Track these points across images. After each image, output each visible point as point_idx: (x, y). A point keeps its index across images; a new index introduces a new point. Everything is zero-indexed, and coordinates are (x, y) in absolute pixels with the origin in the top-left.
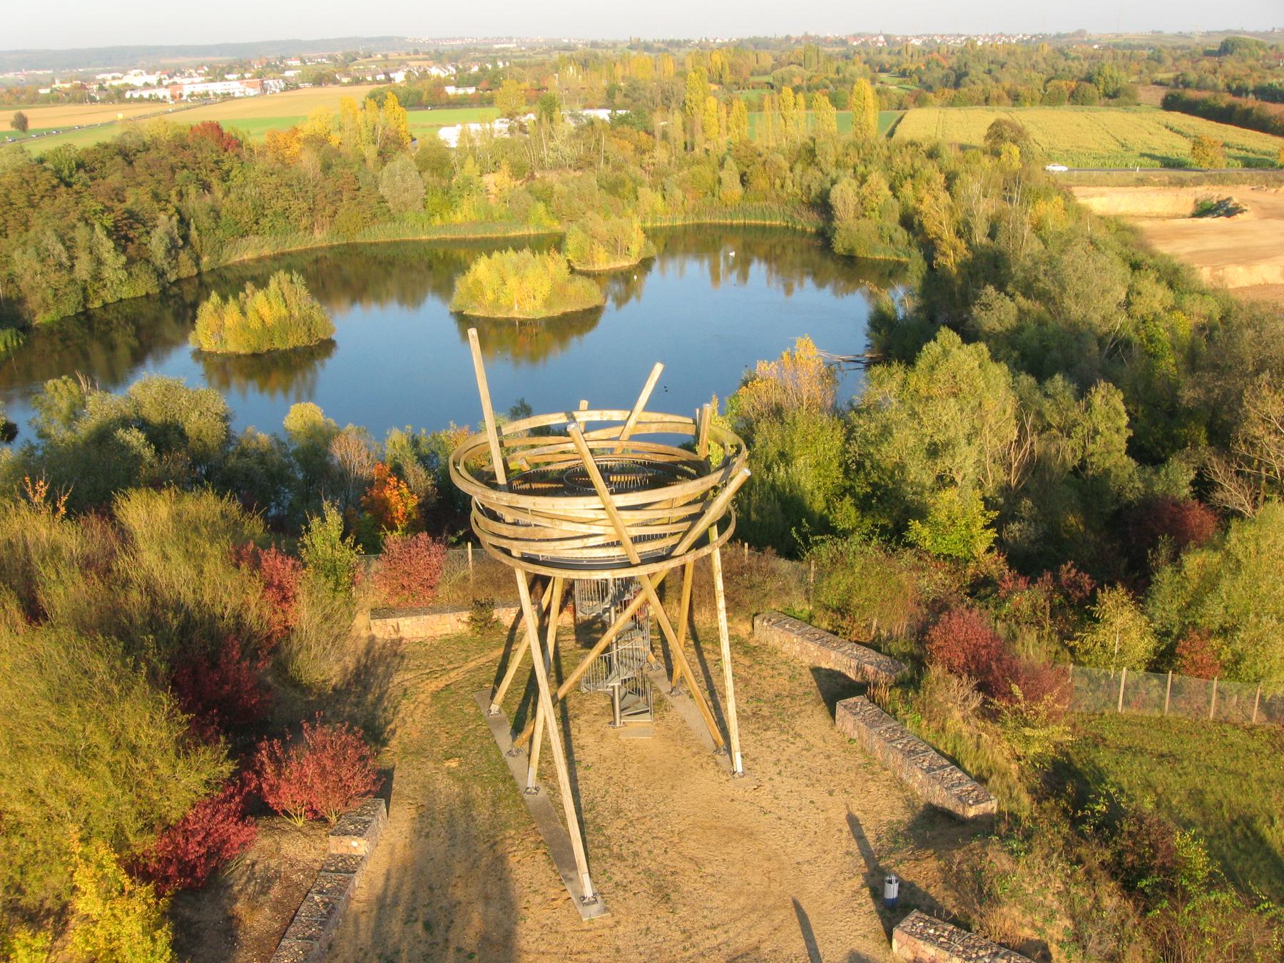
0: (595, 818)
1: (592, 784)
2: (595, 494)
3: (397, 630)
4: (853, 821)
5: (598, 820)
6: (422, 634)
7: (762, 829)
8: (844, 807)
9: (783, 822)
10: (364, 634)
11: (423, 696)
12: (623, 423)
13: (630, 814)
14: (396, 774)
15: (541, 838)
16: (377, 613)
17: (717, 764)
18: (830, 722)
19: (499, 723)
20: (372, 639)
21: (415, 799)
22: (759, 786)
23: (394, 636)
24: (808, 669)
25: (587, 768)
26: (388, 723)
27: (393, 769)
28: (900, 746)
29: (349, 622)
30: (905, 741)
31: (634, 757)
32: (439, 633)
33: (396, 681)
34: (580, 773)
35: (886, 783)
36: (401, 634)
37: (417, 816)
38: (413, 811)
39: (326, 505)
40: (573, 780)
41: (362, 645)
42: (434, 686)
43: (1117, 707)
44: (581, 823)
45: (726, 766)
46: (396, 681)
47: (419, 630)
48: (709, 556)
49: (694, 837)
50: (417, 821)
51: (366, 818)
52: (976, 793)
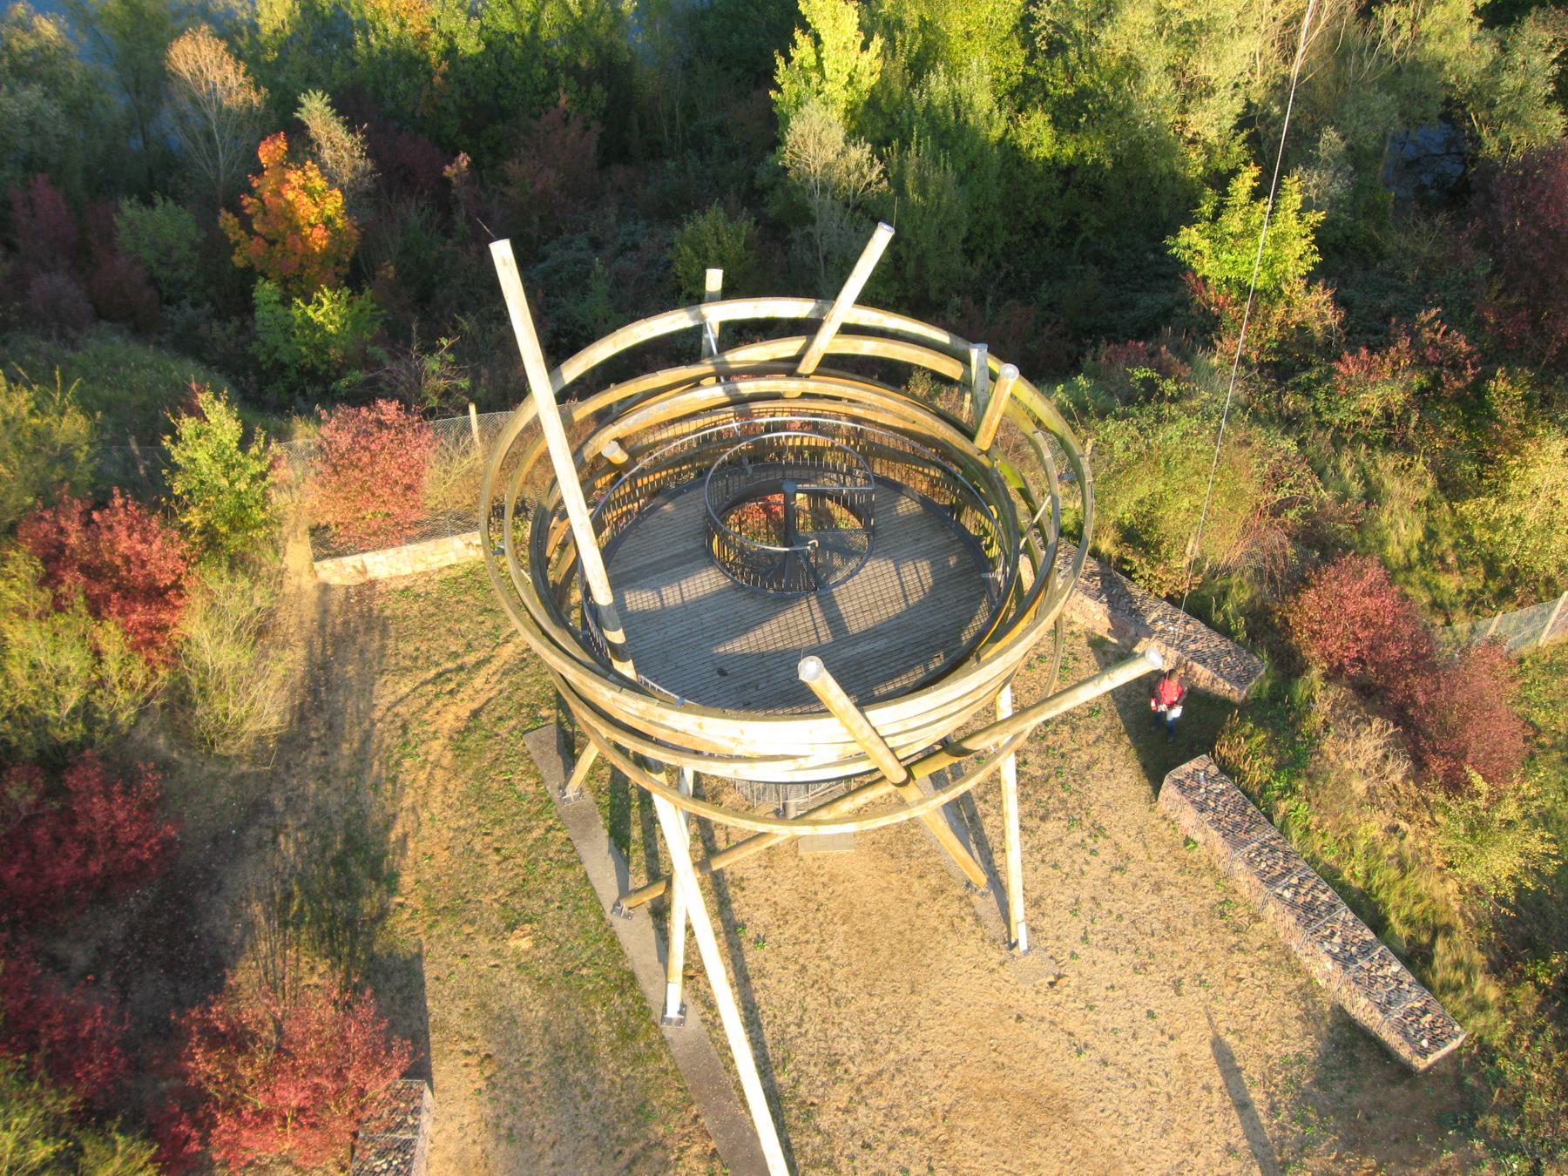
0: (797, 1082)
1: (776, 988)
2: (826, 712)
3: (363, 572)
4: (1224, 1057)
5: (802, 1089)
6: (406, 571)
7: (1081, 1096)
8: (1204, 1022)
9: (1110, 1070)
10: (308, 583)
11: (436, 745)
12: (807, 328)
13: (853, 1069)
14: (429, 971)
15: (713, 1145)
16: (325, 542)
17: (977, 919)
18: (1146, 789)
19: (585, 820)
20: (325, 588)
21: (471, 1038)
22: (1059, 977)
23: (361, 580)
24: (1084, 640)
25: (759, 941)
26: (388, 826)
27: (419, 956)
28: (1287, 894)
29: (277, 564)
30: (1295, 881)
31: (833, 905)
32: (435, 567)
33: (383, 703)
34: (752, 957)
35: (1264, 954)
36: (371, 576)
37: (481, 1084)
38: (475, 1073)
39: (204, 399)
40: (742, 979)
41: (310, 612)
42: (453, 715)
43: (1420, 420)
44: (774, 1098)
45: (994, 927)
46: (383, 703)
47: (400, 565)
48: (865, 299)
49: (971, 1124)
50: (484, 1098)
51: (403, 1135)
52: (1429, 1017)
